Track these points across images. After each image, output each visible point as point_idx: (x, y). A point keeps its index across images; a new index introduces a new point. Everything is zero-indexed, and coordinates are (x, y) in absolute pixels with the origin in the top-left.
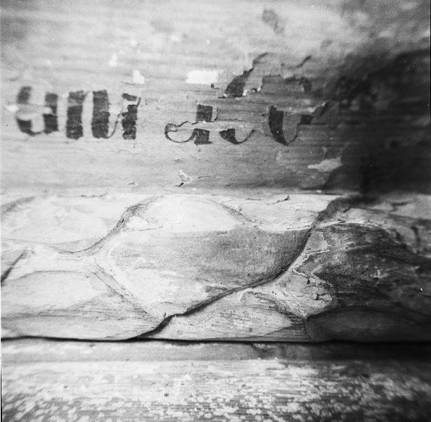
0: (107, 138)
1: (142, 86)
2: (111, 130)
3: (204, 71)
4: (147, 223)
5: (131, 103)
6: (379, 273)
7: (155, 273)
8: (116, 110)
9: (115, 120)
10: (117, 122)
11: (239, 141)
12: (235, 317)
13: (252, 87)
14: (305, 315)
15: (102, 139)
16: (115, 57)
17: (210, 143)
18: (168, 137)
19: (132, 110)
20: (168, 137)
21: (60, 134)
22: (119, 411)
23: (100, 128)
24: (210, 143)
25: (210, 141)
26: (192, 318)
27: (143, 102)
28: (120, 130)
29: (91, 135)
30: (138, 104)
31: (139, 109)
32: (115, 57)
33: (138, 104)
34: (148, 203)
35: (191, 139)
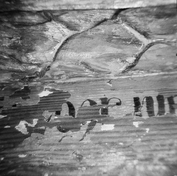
0: (146, 97)
1: (134, 121)
2: (145, 100)
3: (107, 130)
4: (126, 60)
5: (137, 113)
6: (20, 42)
7: (122, 37)
8: (144, 108)
9: (144, 105)
10: (143, 104)
11: (88, 101)
12: (84, 20)
13: (85, 125)
14: (35, 16)
15: (148, 96)
16: (147, 132)
17: (100, 99)
18: (120, 100)
19: (137, 110)
20: (120, 100)
21: (166, 96)
22: (168, 149)
23: (149, 100)
24: (100, 99)
25: (101, 100)
26: (94, 8)
27: (133, 114)
28: (141, 101)
29: (153, 98)
30: (134, 113)
31: (134, 111)
32: (147, 132)
33: (134, 113)
34: (126, 69)
35: (109, 100)
